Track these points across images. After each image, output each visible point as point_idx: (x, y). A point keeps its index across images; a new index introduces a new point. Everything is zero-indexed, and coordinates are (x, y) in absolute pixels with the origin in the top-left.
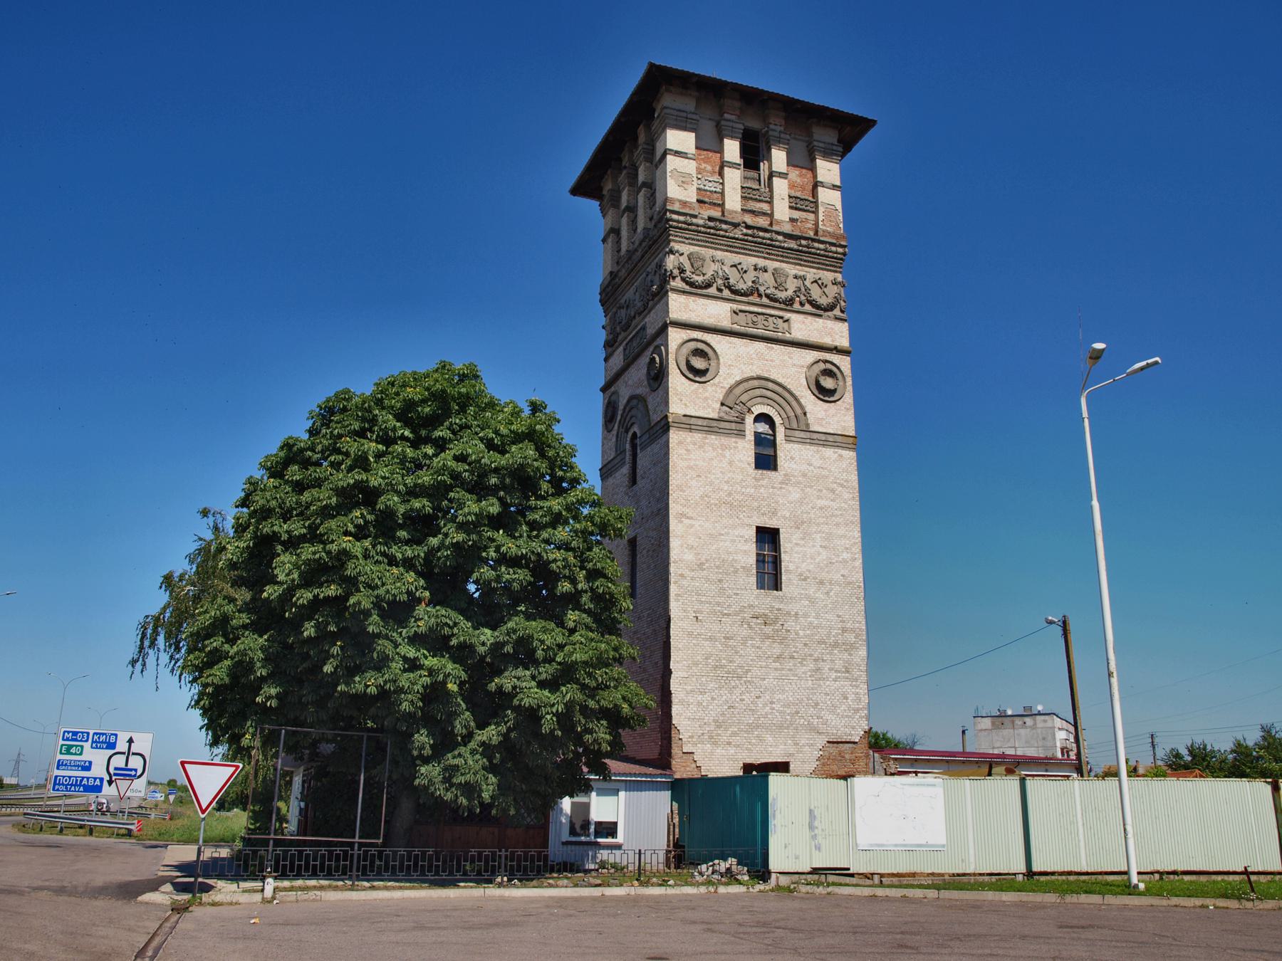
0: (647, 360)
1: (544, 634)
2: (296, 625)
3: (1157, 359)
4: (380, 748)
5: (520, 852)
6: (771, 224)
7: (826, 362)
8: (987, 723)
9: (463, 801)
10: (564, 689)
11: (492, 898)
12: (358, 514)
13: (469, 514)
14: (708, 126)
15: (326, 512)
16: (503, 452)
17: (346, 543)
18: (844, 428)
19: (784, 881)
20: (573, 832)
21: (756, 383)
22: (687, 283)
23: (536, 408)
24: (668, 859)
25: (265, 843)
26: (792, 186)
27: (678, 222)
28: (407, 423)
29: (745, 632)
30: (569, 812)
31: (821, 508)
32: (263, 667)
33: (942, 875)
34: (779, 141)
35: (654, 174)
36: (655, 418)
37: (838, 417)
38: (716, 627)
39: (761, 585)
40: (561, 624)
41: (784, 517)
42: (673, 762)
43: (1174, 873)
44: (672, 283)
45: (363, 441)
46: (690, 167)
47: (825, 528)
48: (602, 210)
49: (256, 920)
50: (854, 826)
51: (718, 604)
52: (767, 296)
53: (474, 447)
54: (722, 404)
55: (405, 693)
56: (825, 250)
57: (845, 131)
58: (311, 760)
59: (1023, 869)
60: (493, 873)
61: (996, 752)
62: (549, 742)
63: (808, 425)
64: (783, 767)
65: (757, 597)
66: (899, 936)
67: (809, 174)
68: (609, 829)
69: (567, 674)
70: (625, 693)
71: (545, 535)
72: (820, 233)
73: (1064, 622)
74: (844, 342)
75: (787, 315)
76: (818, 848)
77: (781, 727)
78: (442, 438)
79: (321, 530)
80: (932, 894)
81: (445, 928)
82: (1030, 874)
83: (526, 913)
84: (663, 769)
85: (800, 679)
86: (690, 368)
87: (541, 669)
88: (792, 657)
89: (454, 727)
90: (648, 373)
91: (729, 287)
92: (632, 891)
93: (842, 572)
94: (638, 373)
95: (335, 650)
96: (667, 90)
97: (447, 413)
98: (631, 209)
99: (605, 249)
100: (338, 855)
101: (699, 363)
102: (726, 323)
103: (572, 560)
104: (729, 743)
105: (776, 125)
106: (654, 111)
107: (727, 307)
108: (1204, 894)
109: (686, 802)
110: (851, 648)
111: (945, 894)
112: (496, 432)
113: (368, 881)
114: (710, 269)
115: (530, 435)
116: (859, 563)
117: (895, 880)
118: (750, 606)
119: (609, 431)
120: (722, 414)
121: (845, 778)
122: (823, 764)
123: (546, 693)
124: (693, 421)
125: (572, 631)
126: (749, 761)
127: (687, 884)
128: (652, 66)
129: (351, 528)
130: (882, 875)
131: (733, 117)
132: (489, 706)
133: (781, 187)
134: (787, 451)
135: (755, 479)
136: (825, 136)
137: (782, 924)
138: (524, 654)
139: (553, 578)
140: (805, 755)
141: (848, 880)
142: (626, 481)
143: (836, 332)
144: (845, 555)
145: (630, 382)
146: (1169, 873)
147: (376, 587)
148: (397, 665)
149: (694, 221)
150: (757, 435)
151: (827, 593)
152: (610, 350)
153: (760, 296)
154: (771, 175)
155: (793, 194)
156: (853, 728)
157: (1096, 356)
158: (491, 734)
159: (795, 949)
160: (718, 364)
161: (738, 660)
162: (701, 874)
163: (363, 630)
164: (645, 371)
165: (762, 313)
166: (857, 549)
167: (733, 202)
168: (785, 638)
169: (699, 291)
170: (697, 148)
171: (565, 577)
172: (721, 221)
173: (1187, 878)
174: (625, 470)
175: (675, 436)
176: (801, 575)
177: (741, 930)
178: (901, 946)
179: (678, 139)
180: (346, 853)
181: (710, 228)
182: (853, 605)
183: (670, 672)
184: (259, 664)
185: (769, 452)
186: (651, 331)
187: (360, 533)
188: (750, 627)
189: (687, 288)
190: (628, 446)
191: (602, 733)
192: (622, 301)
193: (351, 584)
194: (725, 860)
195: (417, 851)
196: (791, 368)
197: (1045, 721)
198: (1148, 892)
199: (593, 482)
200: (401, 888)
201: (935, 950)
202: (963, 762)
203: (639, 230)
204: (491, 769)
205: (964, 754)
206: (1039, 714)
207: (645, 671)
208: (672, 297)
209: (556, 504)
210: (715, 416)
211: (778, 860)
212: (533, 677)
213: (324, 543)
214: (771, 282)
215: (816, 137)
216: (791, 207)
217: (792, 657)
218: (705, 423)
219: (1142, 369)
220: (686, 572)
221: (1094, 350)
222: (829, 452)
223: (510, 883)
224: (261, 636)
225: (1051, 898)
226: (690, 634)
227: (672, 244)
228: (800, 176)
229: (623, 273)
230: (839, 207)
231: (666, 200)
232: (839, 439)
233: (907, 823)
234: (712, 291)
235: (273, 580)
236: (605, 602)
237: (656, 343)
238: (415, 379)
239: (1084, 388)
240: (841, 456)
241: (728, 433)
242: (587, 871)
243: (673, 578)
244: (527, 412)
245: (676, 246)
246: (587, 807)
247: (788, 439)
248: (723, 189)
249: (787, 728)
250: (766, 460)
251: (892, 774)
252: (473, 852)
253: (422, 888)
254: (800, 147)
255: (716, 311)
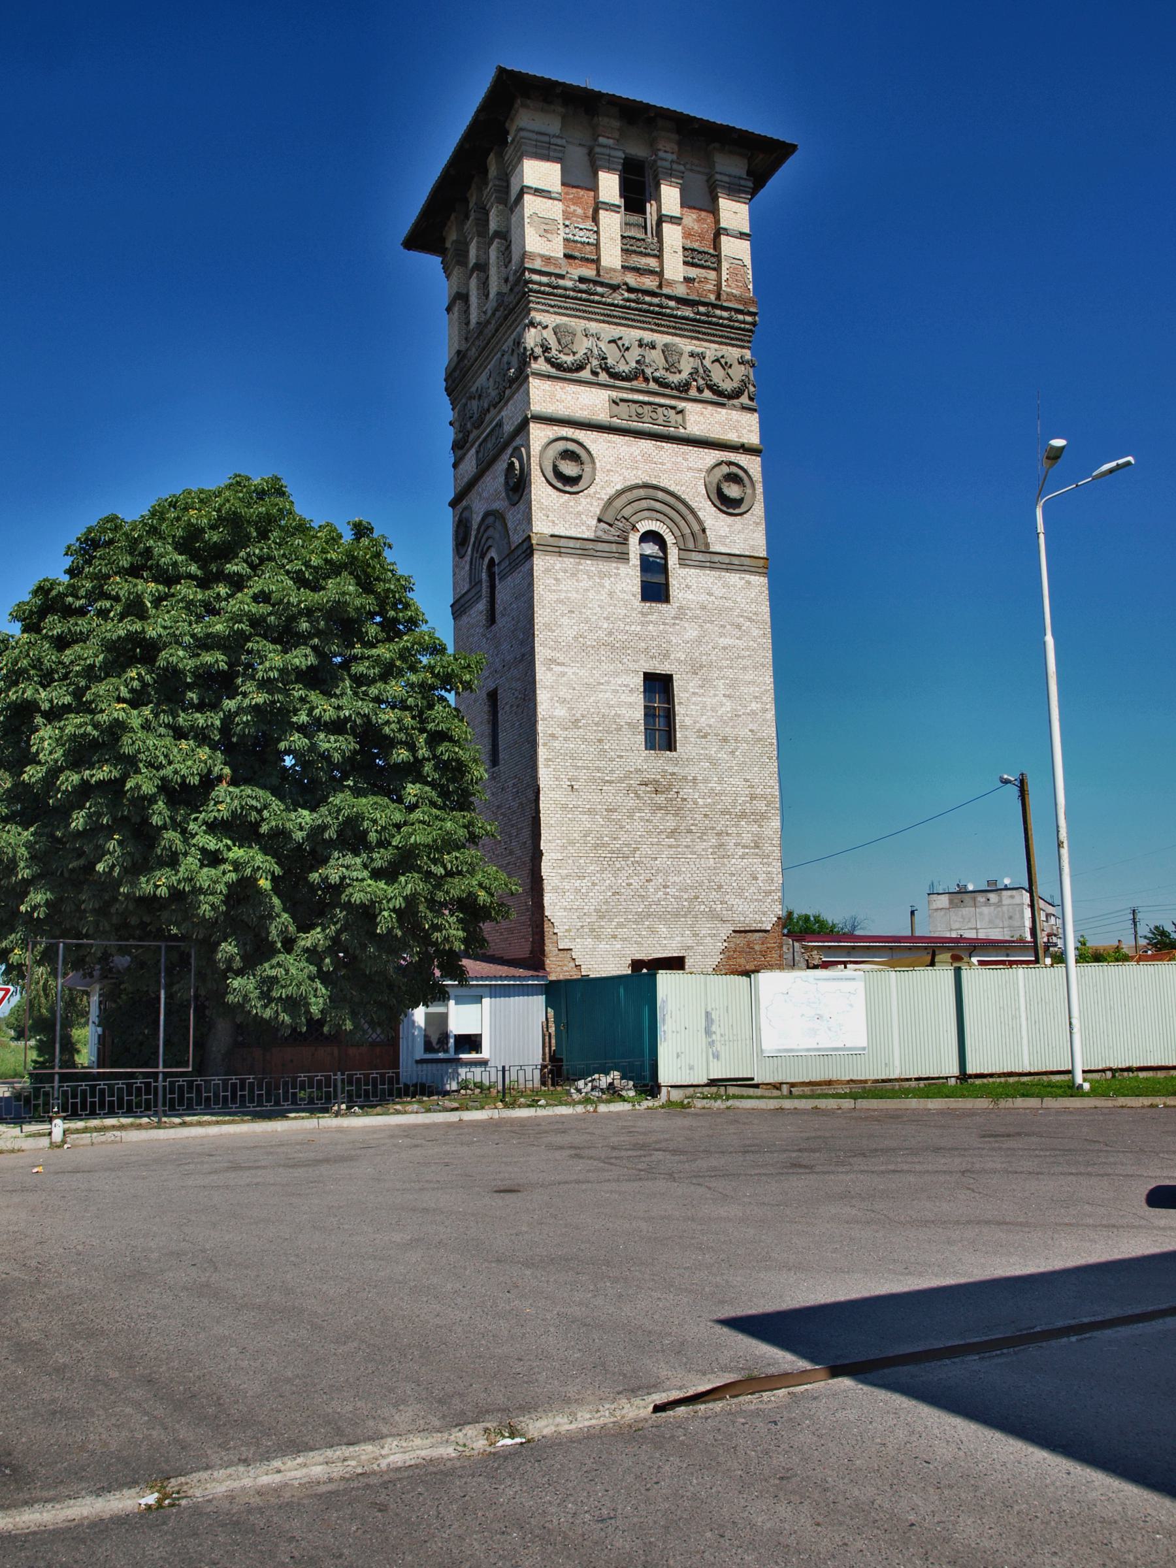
0: (505, 465)
1: (376, 811)
2: (64, 812)
3: (1130, 459)
4: (184, 959)
5: (358, 1074)
6: (660, 286)
7: (730, 464)
8: (943, 901)
9: (285, 1018)
10: (402, 879)
11: (327, 1130)
12: (134, 674)
13: (271, 669)
14: (578, 154)
15: (90, 673)
16: (316, 588)
17: (118, 711)
18: (753, 547)
19: (676, 1095)
20: (428, 1047)
21: (642, 493)
22: (553, 365)
23: (361, 530)
24: (543, 1076)
25: (50, 1078)
26: (687, 235)
27: (540, 284)
28: (194, 556)
29: (631, 802)
30: (422, 1024)
31: (724, 648)
32: (27, 867)
33: (865, 1081)
34: (670, 174)
35: (509, 220)
36: (516, 539)
37: (745, 534)
38: (596, 798)
39: (650, 745)
40: (400, 800)
41: (679, 661)
42: (547, 962)
43: (1129, 1069)
44: (534, 366)
45: (135, 581)
46: (554, 210)
47: (729, 673)
48: (445, 269)
49: (40, 1169)
50: (759, 1029)
51: (598, 769)
52: (656, 380)
53: (274, 581)
54: (600, 520)
55: (205, 894)
56: (730, 319)
57: (757, 160)
58: (104, 977)
59: (955, 1071)
60: (328, 1099)
61: (954, 935)
62: (388, 943)
63: (707, 545)
64: (676, 963)
65: (646, 760)
66: (794, 1155)
67: (710, 219)
68: (471, 1042)
69: (405, 861)
70: (486, 879)
71: (373, 691)
72: (724, 296)
73: (1022, 782)
74: (754, 439)
75: (681, 405)
76: (717, 1056)
77: (677, 915)
78: (238, 574)
79: (88, 697)
80: (848, 1104)
81: (264, 1167)
82: (964, 1076)
83: (365, 1146)
84: (536, 970)
85: (700, 857)
86: (559, 475)
87: (375, 855)
88: (690, 831)
89: (268, 933)
90: (507, 483)
91: (606, 369)
92: (495, 1114)
93: (751, 726)
94: (495, 481)
95: (111, 845)
96: (524, 105)
97: (245, 541)
98: (482, 267)
99: (450, 320)
100: (139, 1089)
101: (569, 469)
102: (603, 417)
103: (408, 721)
104: (614, 937)
105: (667, 151)
106: (507, 133)
107: (604, 395)
108: (1155, 1093)
109: (564, 1011)
110: (760, 818)
111: (863, 1104)
112: (307, 564)
113: (212, 1114)
114: (582, 346)
115: (351, 565)
116: (771, 715)
117: (807, 1090)
118: (638, 771)
119: (462, 557)
120: (600, 533)
121: (747, 973)
122: (729, 958)
123: (382, 884)
124: (563, 542)
125: (412, 808)
126: (638, 957)
127: (561, 1103)
128: (502, 72)
129: (124, 692)
130: (793, 1085)
131: (611, 142)
132: (311, 905)
133: (673, 236)
134: (686, 581)
135: (642, 613)
136: (730, 166)
137: (663, 1145)
138: (352, 837)
139: (389, 743)
140: (705, 945)
141: (751, 1091)
142: (483, 619)
143: (745, 427)
144: (754, 706)
145: (485, 495)
146: (1122, 1070)
147: (160, 767)
148: (190, 862)
149: (561, 282)
150: (644, 558)
151: (733, 752)
152: (460, 452)
153: (646, 380)
154: (661, 219)
155: (689, 245)
156: (764, 913)
157: (1055, 455)
158: (315, 937)
159: (671, 1175)
160: (594, 469)
161: (624, 838)
162: (579, 1091)
163: (145, 821)
164: (502, 480)
165: (650, 402)
166: (769, 698)
167: (612, 257)
168: (680, 809)
169: (568, 375)
170: (563, 184)
171: (401, 743)
172: (596, 283)
173: (1142, 1075)
174: (482, 605)
175: (540, 562)
176: (700, 731)
177: (614, 1154)
178: (794, 1165)
179: (539, 173)
180: (148, 1085)
181: (581, 291)
182: (763, 766)
183: (541, 854)
184: (22, 864)
185: (660, 579)
186: (508, 428)
187: (136, 701)
188: (638, 797)
189: (553, 371)
190: (484, 576)
191: (452, 930)
192: (473, 389)
193: (130, 763)
194: (607, 1074)
195: (234, 1079)
196: (686, 473)
197: (1012, 897)
198: (1093, 1093)
199: (438, 621)
200: (217, 1123)
201: (832, 1168)
202: (910, 948)
203: (492, 296)
204: (324, 977)
205: (912, 938)
206: (1006, 888)
207: (511, 853)
208: (534, 382)
209: (384, 652)
210: (589, 534)
211: (668, 1073)
212: (365, 866)
213: (93, 712)
214: (661, 362)
215: (718, 168)
216: (685, 263)
217: (690, 831)
218: (578, 544)
219: (1111, 471)
220: (558, 731)
221: (1052, 447)
222: (734, 578)
223: (349, 1112)
224: (27, 829)
225: (983, 1103)
226: (564, 807)
227: (533, 314)
228: (698, 221)
229: (473, 352)
230: (748, 262)
231: (524, 255)
232: (747, 561)
233: (823, 1021)
234: (585, 374)
235: (34, 760)
236: (455, 770)
237: (514, 444)
238: (201, 501)
239: (1040, 495)
240: (749, 583)
241: (608, 557)
242: (446, 1093)
243: (541, 739)
244: (348, 536)
245: (537, 317)
246: (444, 1017)
247: (683, 562)
248: (598, 240)
249: (685, 916)
250: (655, 589)
251: (815, 967)
252: (302, 1077)
253: (243, 1121)
254: (698, 181)
255: (591, 401)
